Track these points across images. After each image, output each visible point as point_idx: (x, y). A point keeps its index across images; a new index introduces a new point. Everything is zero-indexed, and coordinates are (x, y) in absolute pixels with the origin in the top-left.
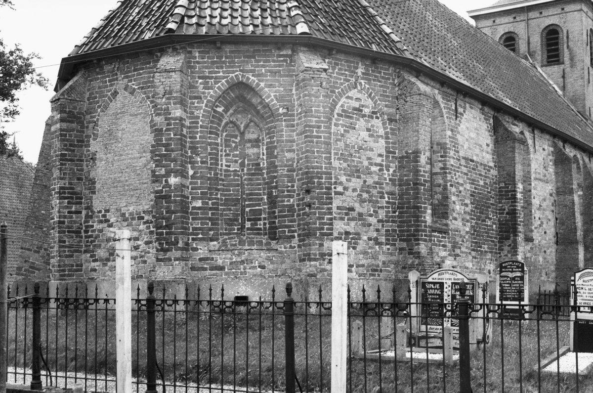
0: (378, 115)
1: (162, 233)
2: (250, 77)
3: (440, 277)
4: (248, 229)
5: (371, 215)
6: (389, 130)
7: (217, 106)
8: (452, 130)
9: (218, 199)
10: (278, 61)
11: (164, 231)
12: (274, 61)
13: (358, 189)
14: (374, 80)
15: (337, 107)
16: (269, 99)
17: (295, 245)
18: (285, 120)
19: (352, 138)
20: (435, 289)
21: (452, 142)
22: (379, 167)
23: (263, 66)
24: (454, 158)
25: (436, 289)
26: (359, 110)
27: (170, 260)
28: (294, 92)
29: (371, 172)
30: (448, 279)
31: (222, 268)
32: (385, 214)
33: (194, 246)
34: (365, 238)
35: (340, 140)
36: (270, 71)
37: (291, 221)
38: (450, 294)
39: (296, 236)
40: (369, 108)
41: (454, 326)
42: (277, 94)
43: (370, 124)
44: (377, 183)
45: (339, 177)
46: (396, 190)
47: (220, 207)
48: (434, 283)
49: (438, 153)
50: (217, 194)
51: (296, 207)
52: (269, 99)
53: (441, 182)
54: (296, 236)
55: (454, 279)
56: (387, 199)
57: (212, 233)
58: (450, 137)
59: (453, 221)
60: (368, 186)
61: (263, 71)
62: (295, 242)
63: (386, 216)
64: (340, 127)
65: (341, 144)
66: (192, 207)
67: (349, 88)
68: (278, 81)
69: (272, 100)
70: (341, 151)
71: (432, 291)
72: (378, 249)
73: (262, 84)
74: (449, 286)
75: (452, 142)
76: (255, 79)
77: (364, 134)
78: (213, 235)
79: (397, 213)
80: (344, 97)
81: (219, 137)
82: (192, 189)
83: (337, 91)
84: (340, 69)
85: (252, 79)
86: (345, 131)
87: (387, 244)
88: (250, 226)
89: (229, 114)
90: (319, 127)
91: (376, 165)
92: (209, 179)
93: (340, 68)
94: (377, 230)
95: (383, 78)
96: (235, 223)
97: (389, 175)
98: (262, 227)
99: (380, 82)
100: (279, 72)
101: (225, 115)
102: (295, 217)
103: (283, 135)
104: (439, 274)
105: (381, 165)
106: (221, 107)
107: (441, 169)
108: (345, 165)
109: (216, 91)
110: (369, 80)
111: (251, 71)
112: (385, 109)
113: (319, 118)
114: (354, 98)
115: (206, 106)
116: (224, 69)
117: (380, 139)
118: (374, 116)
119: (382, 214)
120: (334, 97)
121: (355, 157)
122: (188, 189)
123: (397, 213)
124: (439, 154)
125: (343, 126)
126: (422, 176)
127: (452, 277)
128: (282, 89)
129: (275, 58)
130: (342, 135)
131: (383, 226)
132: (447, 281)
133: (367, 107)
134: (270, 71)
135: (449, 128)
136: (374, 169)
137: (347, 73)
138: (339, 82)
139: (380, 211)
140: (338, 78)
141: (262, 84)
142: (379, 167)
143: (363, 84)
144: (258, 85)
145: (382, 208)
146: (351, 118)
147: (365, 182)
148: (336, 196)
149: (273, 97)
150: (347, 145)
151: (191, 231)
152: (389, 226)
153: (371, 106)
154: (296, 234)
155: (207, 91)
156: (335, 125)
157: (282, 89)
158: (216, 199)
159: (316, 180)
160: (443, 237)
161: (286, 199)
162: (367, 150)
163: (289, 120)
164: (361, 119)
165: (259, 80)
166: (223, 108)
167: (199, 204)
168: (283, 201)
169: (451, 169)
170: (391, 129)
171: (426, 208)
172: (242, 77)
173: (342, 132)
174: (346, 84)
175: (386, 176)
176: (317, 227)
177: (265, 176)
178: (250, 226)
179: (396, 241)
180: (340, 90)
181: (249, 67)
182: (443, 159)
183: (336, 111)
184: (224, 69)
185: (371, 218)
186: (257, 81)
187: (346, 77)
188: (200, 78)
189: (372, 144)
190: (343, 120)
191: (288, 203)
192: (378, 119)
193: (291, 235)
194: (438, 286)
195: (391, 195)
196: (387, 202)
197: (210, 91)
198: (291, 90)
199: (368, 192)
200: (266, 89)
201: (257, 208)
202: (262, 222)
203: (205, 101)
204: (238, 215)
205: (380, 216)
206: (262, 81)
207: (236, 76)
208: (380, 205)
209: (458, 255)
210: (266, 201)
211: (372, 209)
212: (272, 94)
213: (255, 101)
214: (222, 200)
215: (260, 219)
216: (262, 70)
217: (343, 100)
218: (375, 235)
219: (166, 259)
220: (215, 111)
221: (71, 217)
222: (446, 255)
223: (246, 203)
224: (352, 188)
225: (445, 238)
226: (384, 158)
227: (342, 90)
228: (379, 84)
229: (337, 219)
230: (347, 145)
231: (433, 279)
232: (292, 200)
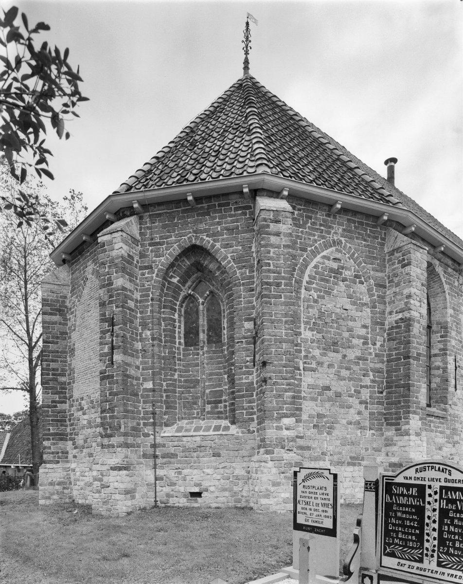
0: (363, 279)
1: (105, 418)
2: (205, 237)
3: (419, 475)
4: (208, 413)
5: (351, 396)
6: (375, 297)
7: (172, 277)
8: (454, 309)
9: (175, 380)
10: (234, 215)
11: (108, 415)
12: (231, 216)
13: (336, 365)
14: (357, 238)
15: (309, 268)
16: (226, 261)
17: (254, 429)
18: (243, 284)
19: (328, 305)
20: (408, 496)
21: (454, 321)
22: (362, 341)
23: (219, 223)
24: (456, 340)
25: (412, 496)
26: (337, 272)
27: (113, 446)
28: (253, 249)
29: (353, 345)
30: (433, 480)
31: (174, 456)
32: (369, 395)
33: (146, 431)
34: (344, 422)
35: (312, 307)
36: (227, 229)
37: (250, 402)
38: (437, 507)
39: (255, 419)
40: (350, 270)
41: (444, 566)
42: (235, 254)
43: (352, 290)
44: (359, 358)
45: (311, 350)
46: (383, 366)
47: (178, 389)
48: (408, 486)
49: (438, 333)
50: (173, 375)
51: (255, 385)
52: (226, 261)
53: (441, 364)
54: (255, 419)
55: (446, 480)
56: (372, 377)
57: (166, 417)
58: (451, 316)
59: (453, 406)
60: (349, 361)
61: (219, 229)
62: (253, 426)
63: (371, 397)
64: (313, 292)
65: (314, 312)
66: (144, 389)
67: (325, 246)
68: (236, 239)
69: (229, 262)
70: (314, 320)
71: (403, 500)
72: (359, 434)
73: (218, 245)
74: (436, 493)
75: (454, 321)
76: (210, 239)
77: (345, 302)
78: (167, 420)
79: (384, 394)
80: (319, 256)
81: (175, 311)
82: (143, 369)
83: (309, 249)
84: (314, 224)
85: (207, 241)
86: (319, 297)
87: (371, 429)
88: (210, 409)
89: (187, 285)
90: (278, 285)
91: (359, 337)
92: (164, 358)
93: (314, 222)
94: (359, 413)
95: (369, 236)
96: (195, 406)
97: (375, 349)
98: (222, 410)
99: (365, 240)
100: (237, 227)
101: (183, 288)
102: (254, 397)
103: (241, 301)
104: (417, 471)
105: (366, 338)
106: (175, 277)
107: (440, 350)
108: (319, 336)
109: (167, 258)
110: (351, 238)
111: (205, 231)
112: (372, 272)
113: (278, 273)
114: (332, 258)
115: (157, 276)
116: (176, 232)
117: (364, 308)
118: (358, 280)
119: (365, 394)
120: (305, 256)
121: (331, 327)
122: (139, 369)
123: (384, 394)
124: (439, 334)
125: (316, 290)
126: (416, 348)
127: (443, 476)
128: (240, 248)
129: (233, 212)
130: (316, 301)
131: (366, 408)
132: (431, 483)
133: (347, 269)
134: (227, 229)
135: (451, 306)
136: (355, 341)
137: (322, 228)
138: (312, 238)
139: (363, 391)
140: (310, 234)
141: (218, 245)
142: (362, 341)
143: (343, 242)
144: (213, 246)
145: (366, 387)
146: (327, 281)
147: (345, 356)
148: (306, 373)
149: (229, 258)
150: (321, 314)
151: (142, 415)
152: (376, 408)
153: (353, 268)
154: (255, 417)
155: (158, 259)
156: (305, 289)
157: (240, 248)
158: (170, 380)
159: (273, 350)
160: (440, 423)
161: (244, 376)
162: (348, 320)
163: (248, 284)
164: (341, 283)
165: (214, 240)
166: (178, 278)
167: (149, 385)
168: (242, 379)
169: (452, 351)
170: (379, 296)
171: (419, 387)
172: (195, 239)
173: (316, 298)
174: (321, 242)
175: (372, 351)
176: (274, 407)
177: (226, 352)
178: (210, 409)
179: (383, 426)
180: (313, 248)
181: (202, 226)
182: (443, 339)
183: (308, 272)
184: (176, 232)
185: (351, 399)
186: (212, 242)
187: (322, 233)
188: (150, 245)
189: (353, 313)
190: (317, 284)
191: (247, 381)
192: (363, 284)
193: (249, 418)
194: (414, 491)
195: (378, 372)
196: (373, 381)
197: (161, 258)
198: (251, 247)
199: (348, 369)
200: (222, 250)
201: (218, 389)
202: (222, 405)
203: (156, 270)
204: (197, 398)
205: (363, 397)
206: (217, 241)
207: (189, 238)
208: (363, 384)
209: (458, 442)
210: (226, 380)
211: (353, 389)
212: (229, 255)
213: (212, 266)
214: (180, 381)
215: (220, 402)
216: (217, 228)
217: (318, 258)
218: (357, 418)
219: (110, 445)
220: (169, 283)
221: (56, 406)
222: (443, 442)
223: (207, 384)
224: (328, 363)
225: (443, 424)
226: (370, 330)
227: (316, 248)
228: (364, 243)
229: (308, 398)
230: (321, 314)
231: (406, 478)
232: (250, 377)
